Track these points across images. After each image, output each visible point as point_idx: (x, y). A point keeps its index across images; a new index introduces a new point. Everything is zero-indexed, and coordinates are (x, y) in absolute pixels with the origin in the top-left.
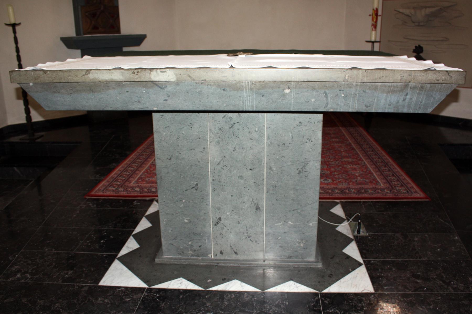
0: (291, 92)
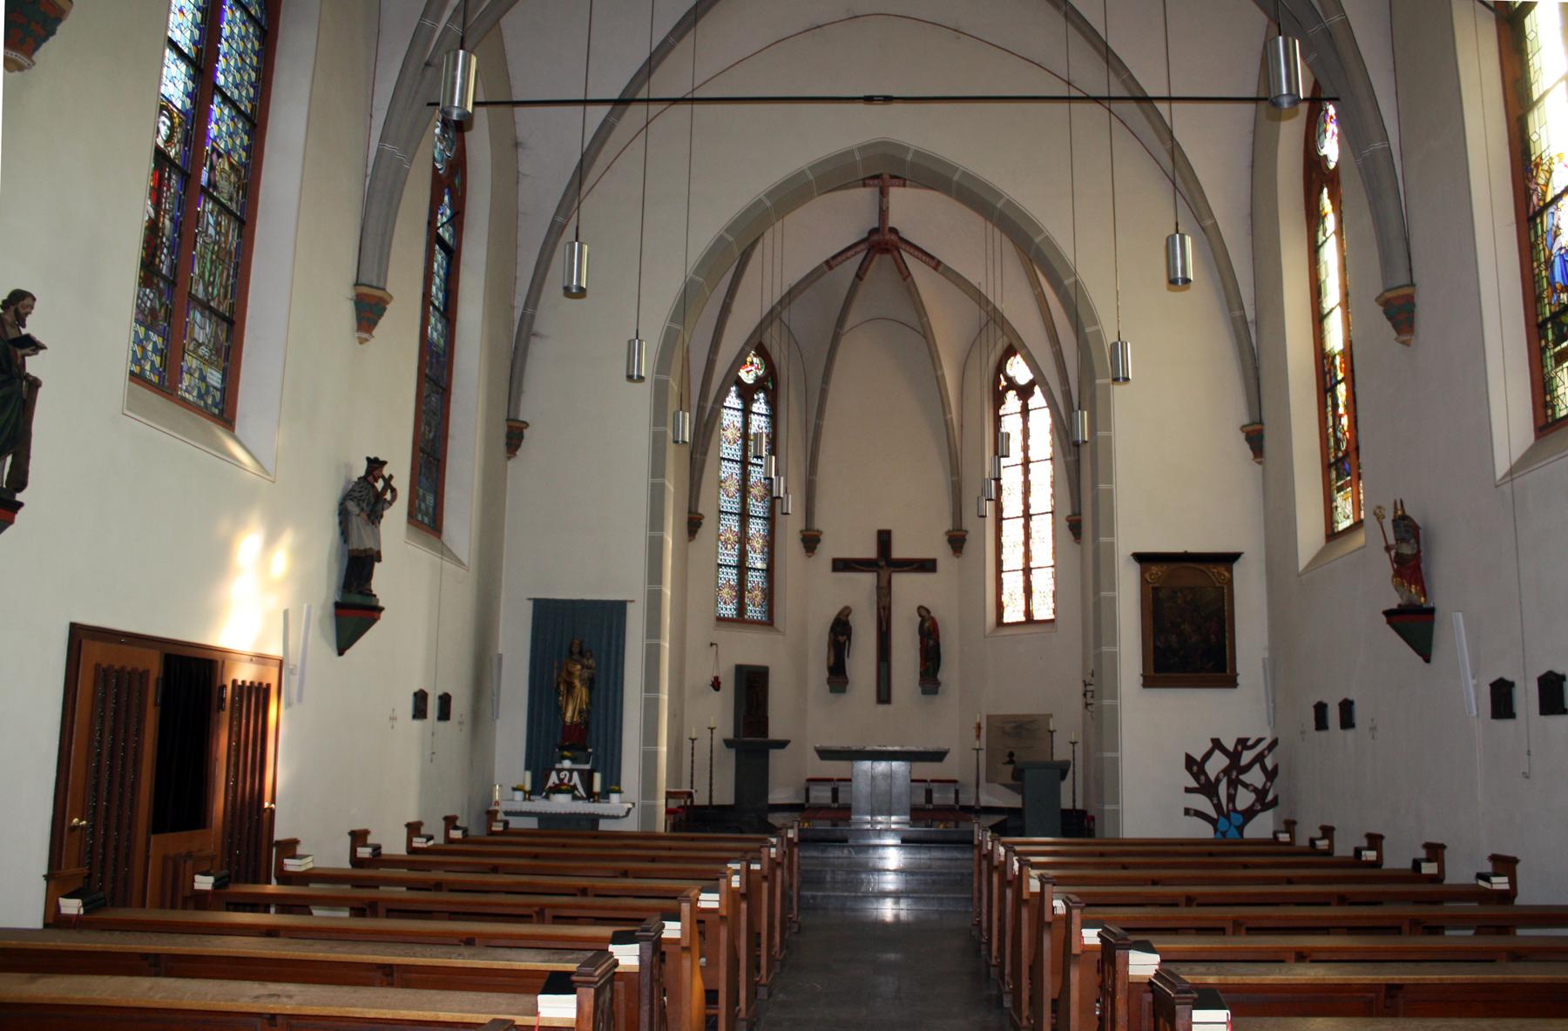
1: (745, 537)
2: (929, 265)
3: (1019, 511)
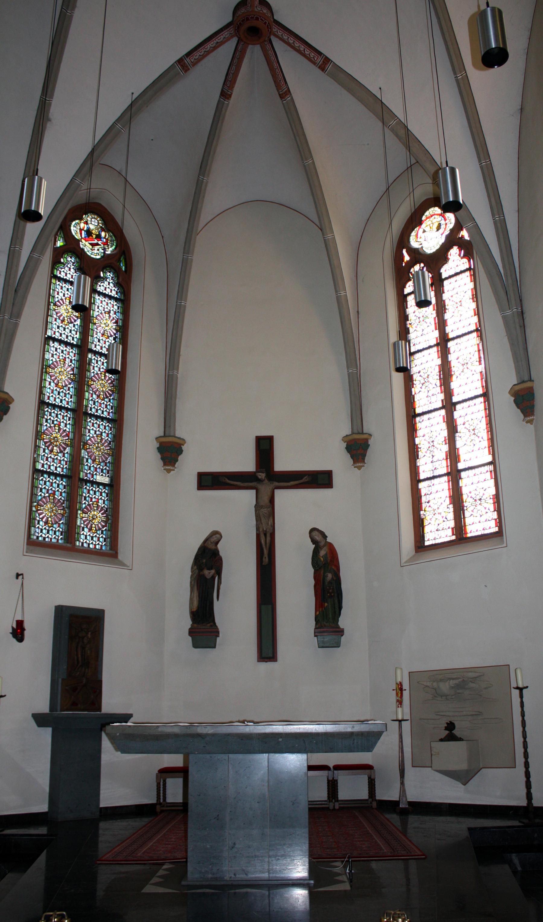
0: (283, 740)
1: (80, 441)
2: (314, 63)
3: (438, 399)
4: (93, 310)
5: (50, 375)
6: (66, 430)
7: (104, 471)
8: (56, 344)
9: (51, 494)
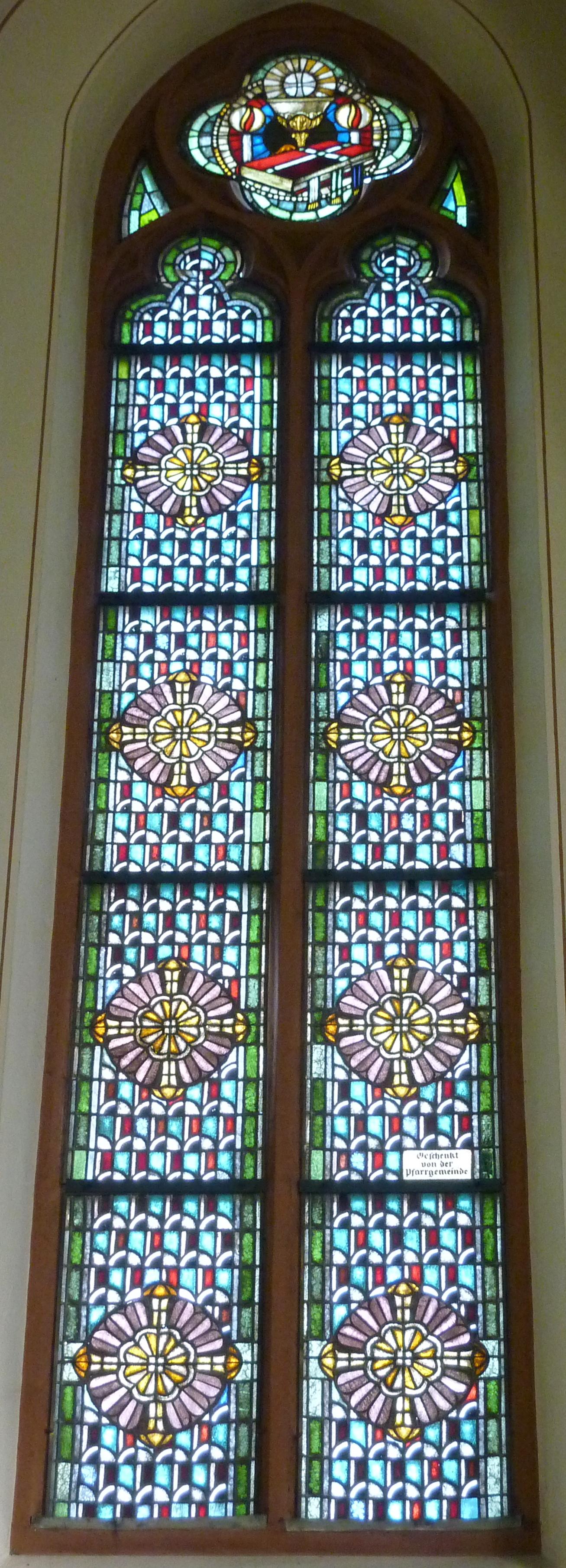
4: (321, 429)
5: (125, 756)
6: (218, 974)
7: (444, 1123)
8: (149, 618)
9: (154, 1285)
